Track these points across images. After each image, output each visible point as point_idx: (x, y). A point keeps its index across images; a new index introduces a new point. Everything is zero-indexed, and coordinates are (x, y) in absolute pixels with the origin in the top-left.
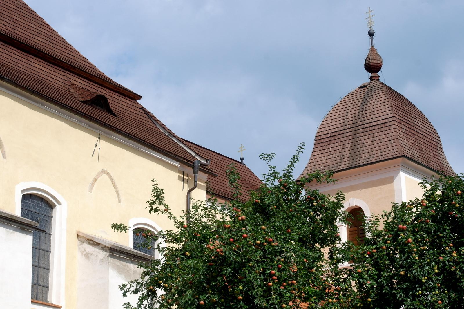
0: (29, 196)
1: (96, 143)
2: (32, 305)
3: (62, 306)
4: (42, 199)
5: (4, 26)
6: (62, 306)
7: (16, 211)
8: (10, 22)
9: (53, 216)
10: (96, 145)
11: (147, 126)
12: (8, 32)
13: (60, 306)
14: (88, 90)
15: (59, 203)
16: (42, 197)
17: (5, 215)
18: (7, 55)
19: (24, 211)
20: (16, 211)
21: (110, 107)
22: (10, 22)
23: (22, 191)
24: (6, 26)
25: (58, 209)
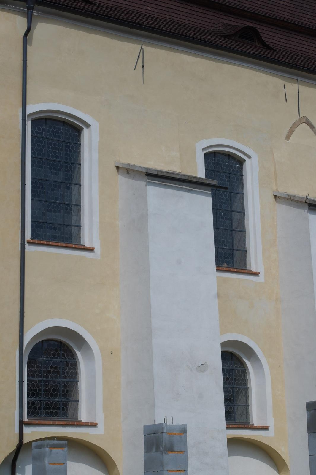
0: (214, 153)
1: (138, 55)
2: (217, 273)
3: (259, 272)
4: (229, 156)
5: (307, 20)
6: (259, 272)
7: (201, 173)
8: (312, 14)
9: (81, 142)
10: (139, 57)
11: (281, 48)
12: (311, 24)
13: (92, 248)
14: (229, 25)
15: (249, 157)
16: (64, 120)
17: (186, 178)
18: (314, 48)
19: (208, 170)
20: (201, 173)
21: (265, 42)
22: (312, 14)
23: (204, 149)
24: (310, 19)
25: (86, 132)
